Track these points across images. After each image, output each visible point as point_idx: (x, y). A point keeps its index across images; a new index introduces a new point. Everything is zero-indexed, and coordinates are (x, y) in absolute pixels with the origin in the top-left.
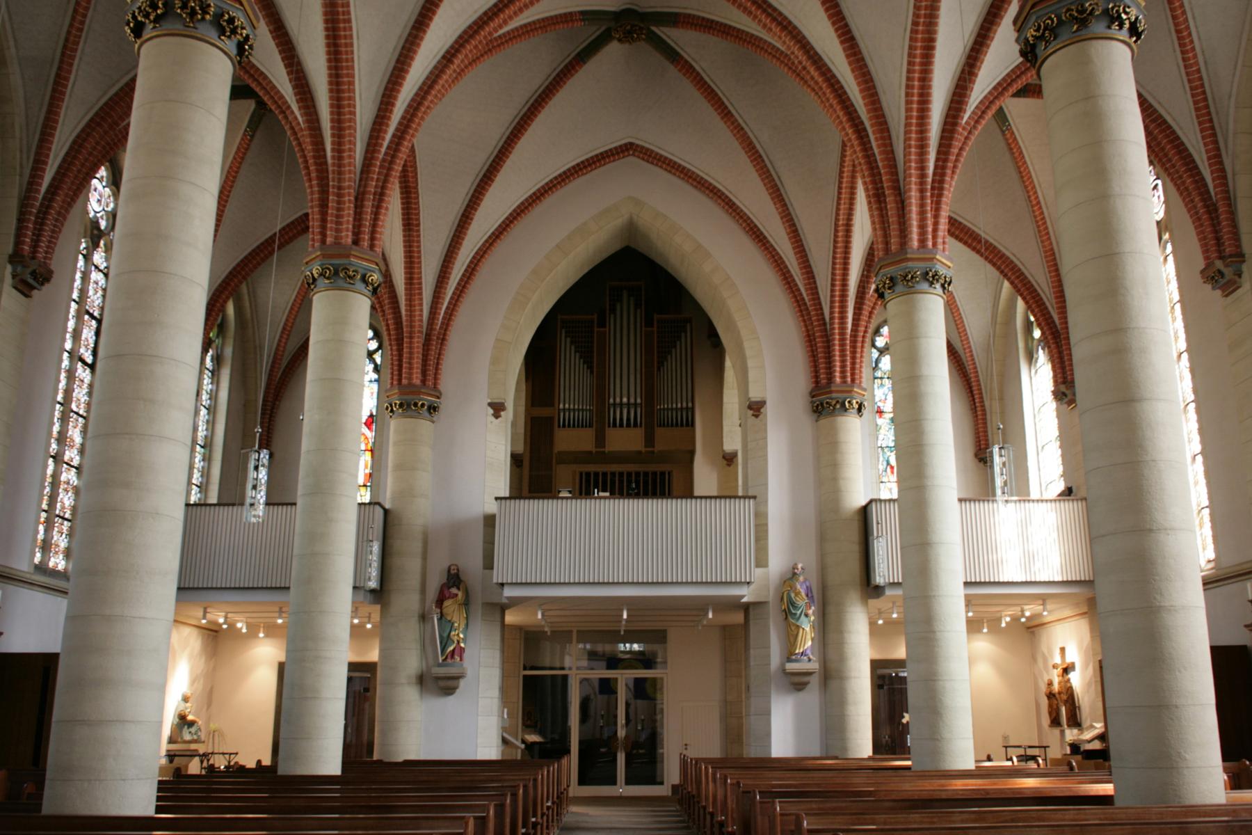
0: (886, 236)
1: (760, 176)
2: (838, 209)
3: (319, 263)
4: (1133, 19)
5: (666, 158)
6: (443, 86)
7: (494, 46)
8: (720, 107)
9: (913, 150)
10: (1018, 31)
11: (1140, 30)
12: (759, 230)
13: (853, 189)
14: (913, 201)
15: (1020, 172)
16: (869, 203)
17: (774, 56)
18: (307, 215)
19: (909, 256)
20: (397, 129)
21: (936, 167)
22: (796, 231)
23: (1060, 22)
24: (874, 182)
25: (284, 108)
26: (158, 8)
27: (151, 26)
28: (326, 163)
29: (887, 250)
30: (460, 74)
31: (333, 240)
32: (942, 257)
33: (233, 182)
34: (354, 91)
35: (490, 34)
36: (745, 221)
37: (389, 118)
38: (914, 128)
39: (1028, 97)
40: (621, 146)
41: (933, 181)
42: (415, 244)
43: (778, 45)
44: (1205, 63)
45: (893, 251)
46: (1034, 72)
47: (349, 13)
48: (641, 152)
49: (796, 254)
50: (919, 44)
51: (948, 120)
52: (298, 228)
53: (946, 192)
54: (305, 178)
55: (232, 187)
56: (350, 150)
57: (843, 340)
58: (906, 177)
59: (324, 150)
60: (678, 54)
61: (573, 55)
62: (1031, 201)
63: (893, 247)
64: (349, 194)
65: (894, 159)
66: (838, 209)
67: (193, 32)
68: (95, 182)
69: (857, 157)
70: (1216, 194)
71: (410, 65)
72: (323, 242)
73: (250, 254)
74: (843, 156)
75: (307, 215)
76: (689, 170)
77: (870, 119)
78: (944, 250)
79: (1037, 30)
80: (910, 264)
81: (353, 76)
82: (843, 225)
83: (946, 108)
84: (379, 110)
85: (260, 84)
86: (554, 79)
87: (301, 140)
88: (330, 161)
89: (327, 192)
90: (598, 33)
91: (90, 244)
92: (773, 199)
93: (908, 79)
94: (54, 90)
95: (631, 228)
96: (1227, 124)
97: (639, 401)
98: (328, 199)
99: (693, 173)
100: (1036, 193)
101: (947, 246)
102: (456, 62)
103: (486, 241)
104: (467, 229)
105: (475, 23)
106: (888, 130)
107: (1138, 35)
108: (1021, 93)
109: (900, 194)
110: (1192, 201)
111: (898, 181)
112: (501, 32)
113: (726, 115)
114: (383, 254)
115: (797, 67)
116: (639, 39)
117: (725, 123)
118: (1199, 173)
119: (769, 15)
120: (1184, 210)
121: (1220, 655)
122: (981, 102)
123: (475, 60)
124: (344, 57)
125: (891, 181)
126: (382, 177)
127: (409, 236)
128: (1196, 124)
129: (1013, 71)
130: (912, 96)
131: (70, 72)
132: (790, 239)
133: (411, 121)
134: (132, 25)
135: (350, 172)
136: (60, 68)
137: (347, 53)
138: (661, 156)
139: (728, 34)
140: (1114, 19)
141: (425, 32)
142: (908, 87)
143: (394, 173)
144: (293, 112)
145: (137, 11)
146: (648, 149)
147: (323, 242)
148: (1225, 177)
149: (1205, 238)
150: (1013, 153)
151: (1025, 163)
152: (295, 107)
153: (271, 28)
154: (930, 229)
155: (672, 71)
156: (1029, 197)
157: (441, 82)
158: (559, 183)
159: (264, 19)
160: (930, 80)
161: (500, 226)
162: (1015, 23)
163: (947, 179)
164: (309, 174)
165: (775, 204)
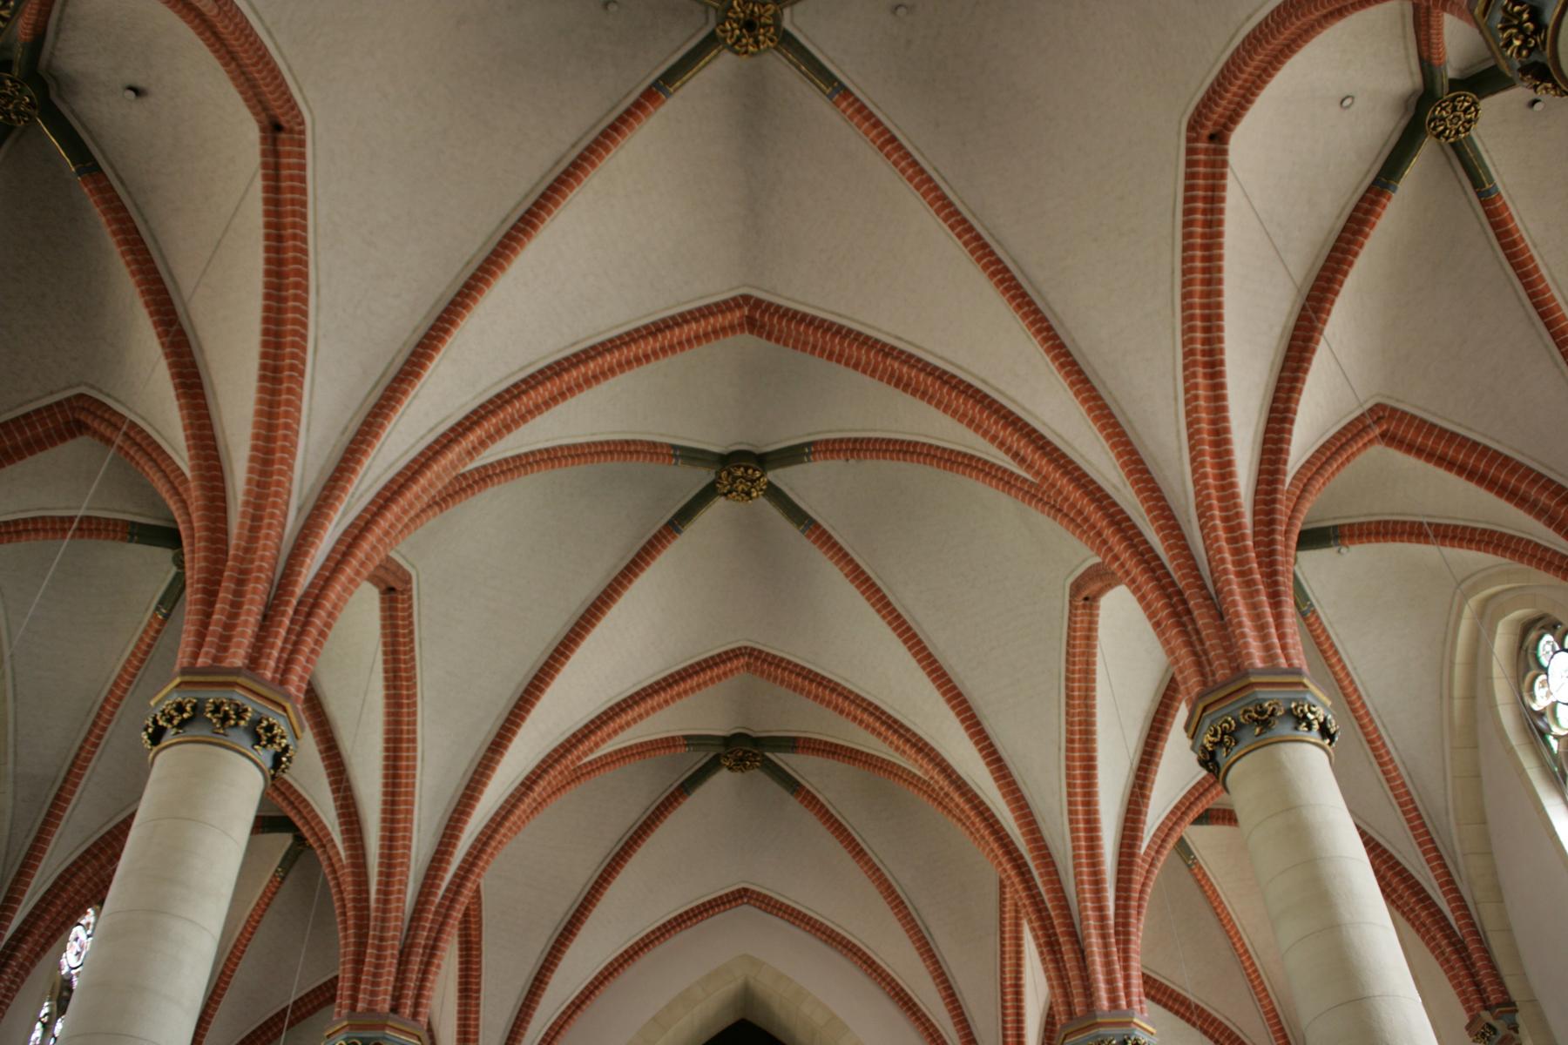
0: (1067, 995)
1: (904, 925)
2: (1003, 966)
3: (344, 1036)
4: (1322, 719)
5: (788, 907)
6: (519, 818)
7: (579, 775)
8: (850, 843)
9: (1087, 887)
10: (1192, 737)
11: (1332, 731)
12: (906, 994)
13: (1018, 940)
14: (1095, 949)
15: (1218, 914)
16: (1041, 953)
17: (910, 783)
18: (337, 978)
19: (1099, 1020)
20: (460, 868)
21: (1117, 907)
22: (952, 995)
23: (1240, 726)
24: (1043, 927)
25: (325, 841)
26: (185, 711)
27: (174, 731)
28: (368, 908)
29: (1070, 1013)
30: (540, 805)
31: (365, 1005)
32: (1142, 1020)
33: (252, 934)
34: (411, 821)
35: (573, 762)
36: (889, 984)
37: (451, 854)
38: (1084, 861)
39: (1212, 824)
40: (733, 893)
41: (1116, 924)
42: (473, 1016)
43: (915, 770)
44: (1409, 774)
45: (1079, 1014)
46: (1220, 787)
47: (414, 732)
48: (757, 900)
49: (955, 1024)
50: (1077, 764)
51: (1124, 850)
52: (323, 995)
53: (1133, 938)
54: (340, 927)
55: (249, 940)
56: (400, 892)
58: (1083, 919)
59: (367, 892)
60: (798, 784)
61: (676, 785)
62: (1236, 950)
63: (1078, 1009)
64: (393, 947)
65: (1065, 898)
66: (1003, 966)
67: (221, 739)
68: (77, 931)
69: (1020, 897)
70: (1460, 929)
71: (481, 792)
72: (353, 1008)
73: (260, 1027)
74: (1002, 899)
75: (337, 978)
76: (816, 921)
77: (1031, 851)
78: (1142, 1011)
79: (1215, 735)
80: (1102, 1030)
81: (412, 804)
82: (1011, 985)
83: (1119, 836)
84: (441, 843)
85: (299, 812)
86: (653, 813)
87: (341, 879)
88: (373, 904)
89: (365, 945)
90: (704, 761)
91: (55, 1009)
92: (921, 954)
93: (1070, 803)
94: (49, 814)
95: (747, 997)
96: (1452, 845)
98: (365, 952)
99: (822, 924)
100: (1240, 939)
101: (1144, 1006)
102: (537, 789)
103: (564, 1013)
104: (540, 996)
105: (562, 745)
106: (1053, 864)
107: (1332, 737)
108: (1206, 818)
109: (1078, 942)
110: (1433, 938)
111: (1072, 925)
112: (591, 757)
113: (858, 853)
114: (429, 1024)
115: (938, 794)
116: (752, 767)
117: (858, 862)
118: (1434, 904)
119: (901, 736)
120: (1427, 951)
122: (1159, 829)
123: (557, 791)
124: (404, 781)
125: (1064, 925)
126: (437, 926)
127: (466, 1005)
128: (1417, 847)
129: (1190, 792)
130: (1077, 822)
131: (72, 793)
132: (947, 1005)
133: (477, 857)
134: (150, 730)
135: (397, 918)
136: (61, 789)
137: (407, 776)
138: (782, 904)
139: (855, 759)
140: (1301, 719)
141: (502, 754)
142: (1071, 812)
143: (458, 906)
144: (334, 846)
145: (159, 714)
146: (765, 896)
147: (353, 1008)
148: (1465, 907)
149: (1460, 984)
150: (1205, 892)
151: (1221, 903)
152: (338, 839)
153: (322, 747)
154: (1121, 984)
155: (793, 804)
156: (1234, 944)
157: (517, 812)
158: (657, 938)
159: (312, 728)
160: (1096, 804)
161: (582, 993)
162: (1187, 728)
163: (1133, 921)
164: (345, 922)
165: (924, 960)
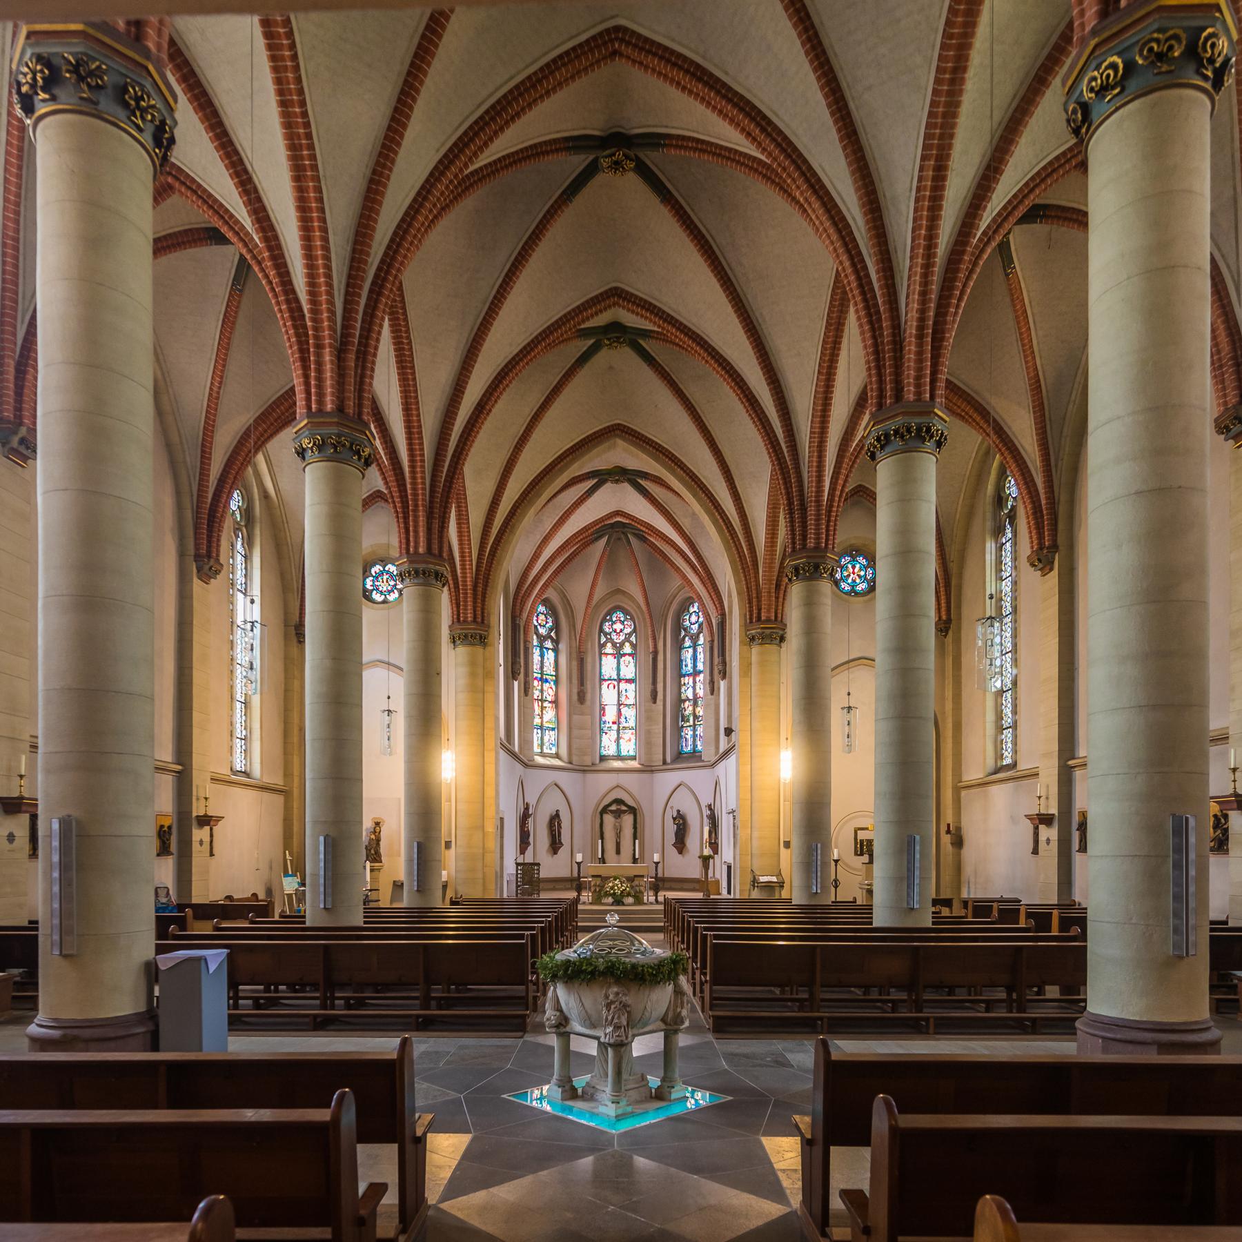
57: (818, 515)
97: (700, 666)
112: (471, 168)
121: (25, 450)
